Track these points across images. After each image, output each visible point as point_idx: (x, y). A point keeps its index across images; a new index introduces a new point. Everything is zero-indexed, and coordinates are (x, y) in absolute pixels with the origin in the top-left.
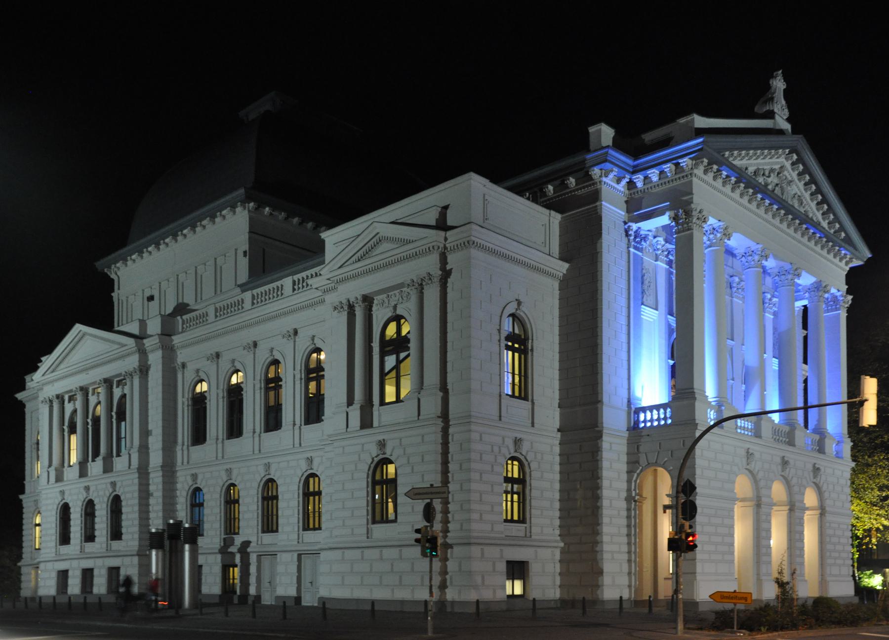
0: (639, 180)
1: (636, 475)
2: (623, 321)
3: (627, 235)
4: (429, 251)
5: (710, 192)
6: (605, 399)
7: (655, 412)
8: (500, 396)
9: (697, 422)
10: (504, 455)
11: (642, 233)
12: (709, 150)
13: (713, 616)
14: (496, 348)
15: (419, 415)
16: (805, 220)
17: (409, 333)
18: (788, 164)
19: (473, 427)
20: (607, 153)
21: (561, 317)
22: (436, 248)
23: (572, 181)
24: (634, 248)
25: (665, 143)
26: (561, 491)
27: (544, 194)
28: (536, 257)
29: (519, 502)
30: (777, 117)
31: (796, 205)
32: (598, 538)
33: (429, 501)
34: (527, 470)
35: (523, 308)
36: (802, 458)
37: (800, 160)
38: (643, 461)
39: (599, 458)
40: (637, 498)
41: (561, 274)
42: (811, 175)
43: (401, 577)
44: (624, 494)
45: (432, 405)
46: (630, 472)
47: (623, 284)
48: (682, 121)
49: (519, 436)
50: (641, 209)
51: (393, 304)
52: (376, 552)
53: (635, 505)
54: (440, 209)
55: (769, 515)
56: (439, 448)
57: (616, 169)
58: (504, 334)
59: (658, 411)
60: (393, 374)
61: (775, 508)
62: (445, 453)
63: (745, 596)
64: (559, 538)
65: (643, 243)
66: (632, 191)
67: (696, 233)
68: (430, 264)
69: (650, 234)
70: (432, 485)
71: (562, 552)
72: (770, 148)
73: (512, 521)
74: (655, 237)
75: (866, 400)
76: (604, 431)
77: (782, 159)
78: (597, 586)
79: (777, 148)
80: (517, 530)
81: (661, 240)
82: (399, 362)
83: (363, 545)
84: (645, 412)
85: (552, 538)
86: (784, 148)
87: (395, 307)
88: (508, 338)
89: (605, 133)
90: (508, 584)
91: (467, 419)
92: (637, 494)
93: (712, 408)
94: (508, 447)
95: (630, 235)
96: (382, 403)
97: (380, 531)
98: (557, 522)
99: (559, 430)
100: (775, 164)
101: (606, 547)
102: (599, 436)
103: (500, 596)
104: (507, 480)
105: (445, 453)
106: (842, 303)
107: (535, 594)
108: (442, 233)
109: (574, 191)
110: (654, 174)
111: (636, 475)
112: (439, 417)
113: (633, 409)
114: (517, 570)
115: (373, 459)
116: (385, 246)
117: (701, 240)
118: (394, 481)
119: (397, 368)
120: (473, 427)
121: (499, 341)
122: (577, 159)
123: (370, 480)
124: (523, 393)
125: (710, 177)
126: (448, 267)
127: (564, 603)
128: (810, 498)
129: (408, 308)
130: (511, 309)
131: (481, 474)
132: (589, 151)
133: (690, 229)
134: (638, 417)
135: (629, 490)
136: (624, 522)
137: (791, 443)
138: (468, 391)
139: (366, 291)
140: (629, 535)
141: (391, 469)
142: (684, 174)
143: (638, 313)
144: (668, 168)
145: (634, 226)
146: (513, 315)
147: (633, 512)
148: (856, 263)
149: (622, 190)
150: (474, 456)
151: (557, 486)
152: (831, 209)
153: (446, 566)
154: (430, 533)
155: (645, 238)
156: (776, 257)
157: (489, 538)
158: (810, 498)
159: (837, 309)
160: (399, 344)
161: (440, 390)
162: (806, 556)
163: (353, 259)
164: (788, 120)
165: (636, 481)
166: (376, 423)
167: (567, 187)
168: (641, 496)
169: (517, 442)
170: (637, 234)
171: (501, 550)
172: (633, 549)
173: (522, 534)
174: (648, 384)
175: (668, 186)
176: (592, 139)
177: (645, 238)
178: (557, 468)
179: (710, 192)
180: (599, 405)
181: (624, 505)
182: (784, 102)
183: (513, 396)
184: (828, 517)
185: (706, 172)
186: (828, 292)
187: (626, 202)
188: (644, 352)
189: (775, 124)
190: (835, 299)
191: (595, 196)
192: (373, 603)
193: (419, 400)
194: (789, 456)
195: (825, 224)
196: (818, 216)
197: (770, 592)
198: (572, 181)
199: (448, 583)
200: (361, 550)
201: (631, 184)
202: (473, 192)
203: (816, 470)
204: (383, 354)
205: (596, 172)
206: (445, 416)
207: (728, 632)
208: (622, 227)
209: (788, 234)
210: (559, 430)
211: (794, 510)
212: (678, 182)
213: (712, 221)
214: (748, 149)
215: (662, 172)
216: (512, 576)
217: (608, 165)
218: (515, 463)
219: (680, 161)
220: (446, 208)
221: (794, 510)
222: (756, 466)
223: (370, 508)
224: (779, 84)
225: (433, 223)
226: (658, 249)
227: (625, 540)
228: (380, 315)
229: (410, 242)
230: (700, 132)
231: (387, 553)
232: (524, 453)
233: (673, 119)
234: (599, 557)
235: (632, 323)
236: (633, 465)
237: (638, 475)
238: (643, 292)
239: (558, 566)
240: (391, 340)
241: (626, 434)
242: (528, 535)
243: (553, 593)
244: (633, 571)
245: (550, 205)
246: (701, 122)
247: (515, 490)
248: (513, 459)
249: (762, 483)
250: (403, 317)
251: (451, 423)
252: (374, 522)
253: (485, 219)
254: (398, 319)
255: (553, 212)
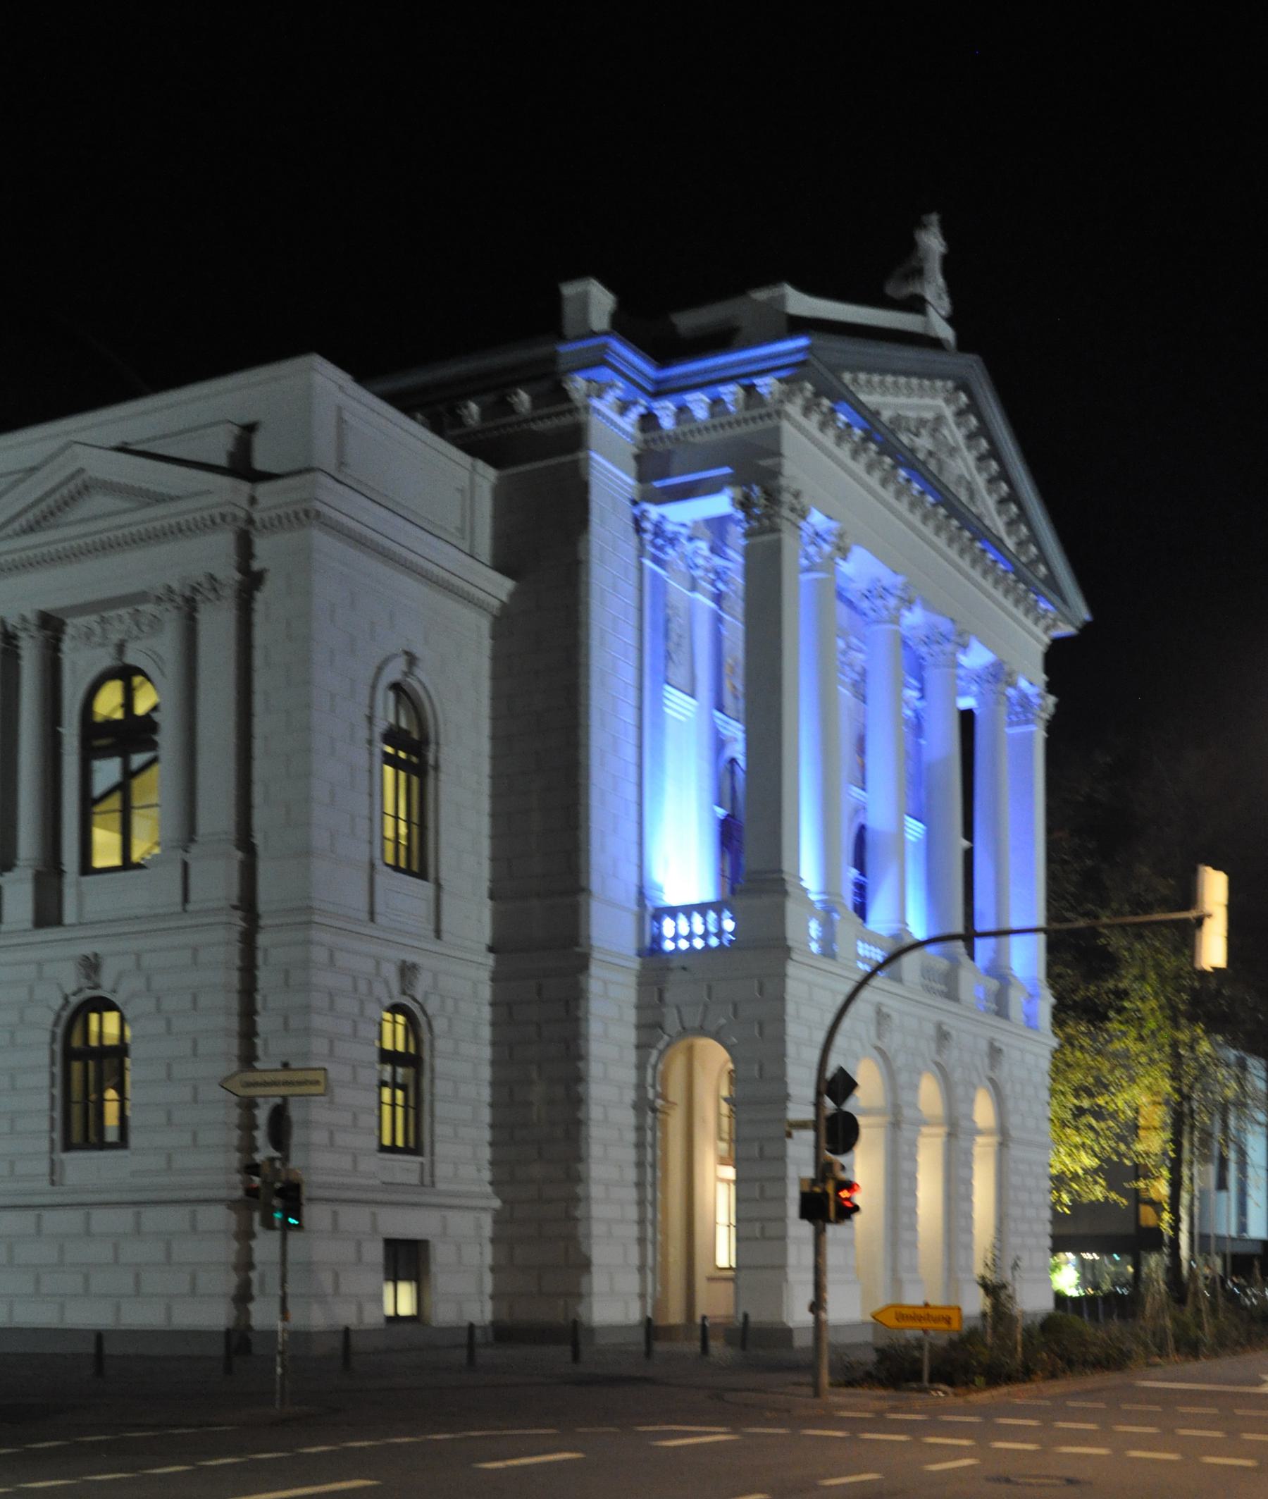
0: (666, 412)
1: (655, 1053)
2: (629, 716)
3: (639, 530)
4: (211, 525)
5: (813, 453)
6: (595, 883)
7: (697, 918)
8: (372, 866)
9: (790, 943)
10: (379, 1000)
11: (669, 528)
12: (821, 368)
13: (872, 1357)
14: (361, 758)
15: (186, 899)
16: (981, 533)
17: (155, 708)
18: (948, 412)
19: (316, 934)
20: (605, 346)
21: (496, 697)
22: (229, 519)
23: (523, 399)
24: (659, 564)
25: (721, 340)
26: (495, 1084)
27: (459, 421)
28: (448, 559)
29: (406, 1107)
30: (931, 311)
31: (964, 497)
32: (580, 1190)
33: (278, 1101)
34: (425, 1036)
35: (420, 673)
36: (972, 1030)
37: (974, 407)
38: (672, 1021)
39: (581, 1014)
40: (659, 1102)
41: (496, 603)
42: (991, 441)
43: (137, 1276)
44: (630, 1095)
45: (216, 879)
46: (643, 1047)
47: (630, 637)
48: (761, 295)
49: (411, 958)
50: (666, 475)
51: (115, 637)
52: (76, 1216)
53: (655, 1118)
54: (236, 430)
55: (913, 1145)
56: (235, 979)
57: (620, 384)
58: (381, 726)
59: (689, 918)
60: (115, 802)
61: (925, 1130)
62: (248, 989)
63: (945, 1313)
64: (489, 1189)
65: (670, 551)
66: (649, 436)
67: (788, 540)
68: (213, 555)
69: (683, 530)
70: (286, 1066)
71: (498, 1219)
72: (921, 375)
73: (393, 1149)
74: (690, 539)
75: (1210, 916)
76: (596, 955)
77: (940, 402)
78: (577, 1295)
79: (931, 376)
80: (405, 1168)
81: (703, 546)
82: (129, 775)
83: (37, 1200)
84: (674, 917)
85: (476, 1189)
86: (944, 377)
87: (121, 648)
88: (389, 737)
89: (597, 301)
90: (388, 1289)
91: (303, 915)
92: (658, 1095)
93: (814, 914)
94: (387, 983)
95: (644, 531)
96: (86, 867)
97: (85, 1168)
98: (486, 1153)
99: (491, 949)
100: (921, 404)
101: (597, 1210)
102: (582, 963)
103: (371, 1319)
104: (388, 1057)
105: (248, 989)
106: (1038, 711)
107: (444, 1314)
108: (245, 487)
109: (526, 421)
110: (698, 404)
111: (655, 1053)
112: (235, 908)
113: (650, 909)
114: (406, 1259)
115: (66, 998)
116: (98, 503)
117: (796, 553)
118: (121, 1050)
119: (123, 788)
120: (316, 934)
121: (370, 742)
122: (540, 351)
123: (58, 1047)
124: (418, 862)
125: (812, 424)
126: (256, 565)
127: (503, 1332)
128: (983, 1111)
129: (157, 648)
130: (394, 672)
131: (331, 1042)
132: (561, 337)
133: (775, 529)
134: (660, 928)
135: (640, 1086)
136: (630, 1155)
137: (952, 994)
138: (305, 853)
139: (50, 603)
140: (640, 1185)
141: (111, 1022)
142: (763, 411)
143: (659, 701)
144: (731, 393)
145: (654, 511)
146: (396, 687)
147: (649, 1134)
148: (1066, 630)
149: (629, 428)
150: (319, 1000)
151: (486, 1073)
152: (1023, 516)
153: (249, 1250)
154: (283, 1176)
155: (672, 541)
156: (927, 606)
157: (348, 1187)
158: (983, 1111)
159: (1028, 722)
160: (133, 734)
161: (239, 848)
162: (920, 1229)
163: (16, 526)
164: (950, 320)
165: (655, 1067)
166: (69, 915)
167: (510, 409)
168: (663, 1097)
169: (407, 971)
170: (659, 531)
171: (335, 1213)
172: (650, 1215)
173: (414, 1179)
174: (673, 855)
175: (729, 432)
176: (569, 311)
177: (672, 541)
178: (486, 1032)
179: (813, 453)
180: (582, 898)
181: (629, 1118)
182: (940, 281)
183: (396, 868)
184: (1015, 1151)
185: (807, 411)
186: (1013, 685)
187: (637, 458)
188: (670, 788)
189: (927, 323)
190: (1025, 701)
191: (574, 438)
192: (99, 1336)
193: (185, 866)
194: (951, 1024)
195: (1010, 543)
196: (998, 524)
197: (974, 1303)
198: (523, 399)
199: (255, 1290)
200: (136, 1209)
201: (649, 421)
202: (316, 398)
203: (995, 1052)
204: (89, 754)
205: (578, 384)
206: (248, 904)
207: (912, 1390)
208: (628, 511)
209: (947, 559)
210: (491, 949)
211: (957, 1132)
212: (752, 427)
213: (817, 518)
214: (883, 371)
215: (716, 402)
216: (394, 1274)
217: (605, 374)
218: (400, 1019)
219: (758, 381)
220: (249, 429)
221: (957, 1132)
222: (893, 1041)
223: (58, 1114)
224: (933, 243)
225: (222, 461)
226: (697, 566)
227: (632, 1194)
228: (81, 661)
229: (161, 499)
230: (798, 325)
231: (104, 1219)
232: (419, 998)
233: (740, 285)
234: (581, 1230)
235: (646, 719)
236: (650, 1031)
237: (661, 1053)
238: (668, 656)
239: (488, 1250)
240: (109, 724)
241: (635, 964)
242: (428, 1181)
243: (481, 1312)
244: (650, 1261)
245: (474, 446)
246: (800, 303)
247: (399, 1080)
248: (395, 1009)
249: (903, 1078)
250: (139, 671)
251: (262, 922)
252: (68, 1146)
253: (342, 464)
254: (126, 674)
255: (480, 464)
